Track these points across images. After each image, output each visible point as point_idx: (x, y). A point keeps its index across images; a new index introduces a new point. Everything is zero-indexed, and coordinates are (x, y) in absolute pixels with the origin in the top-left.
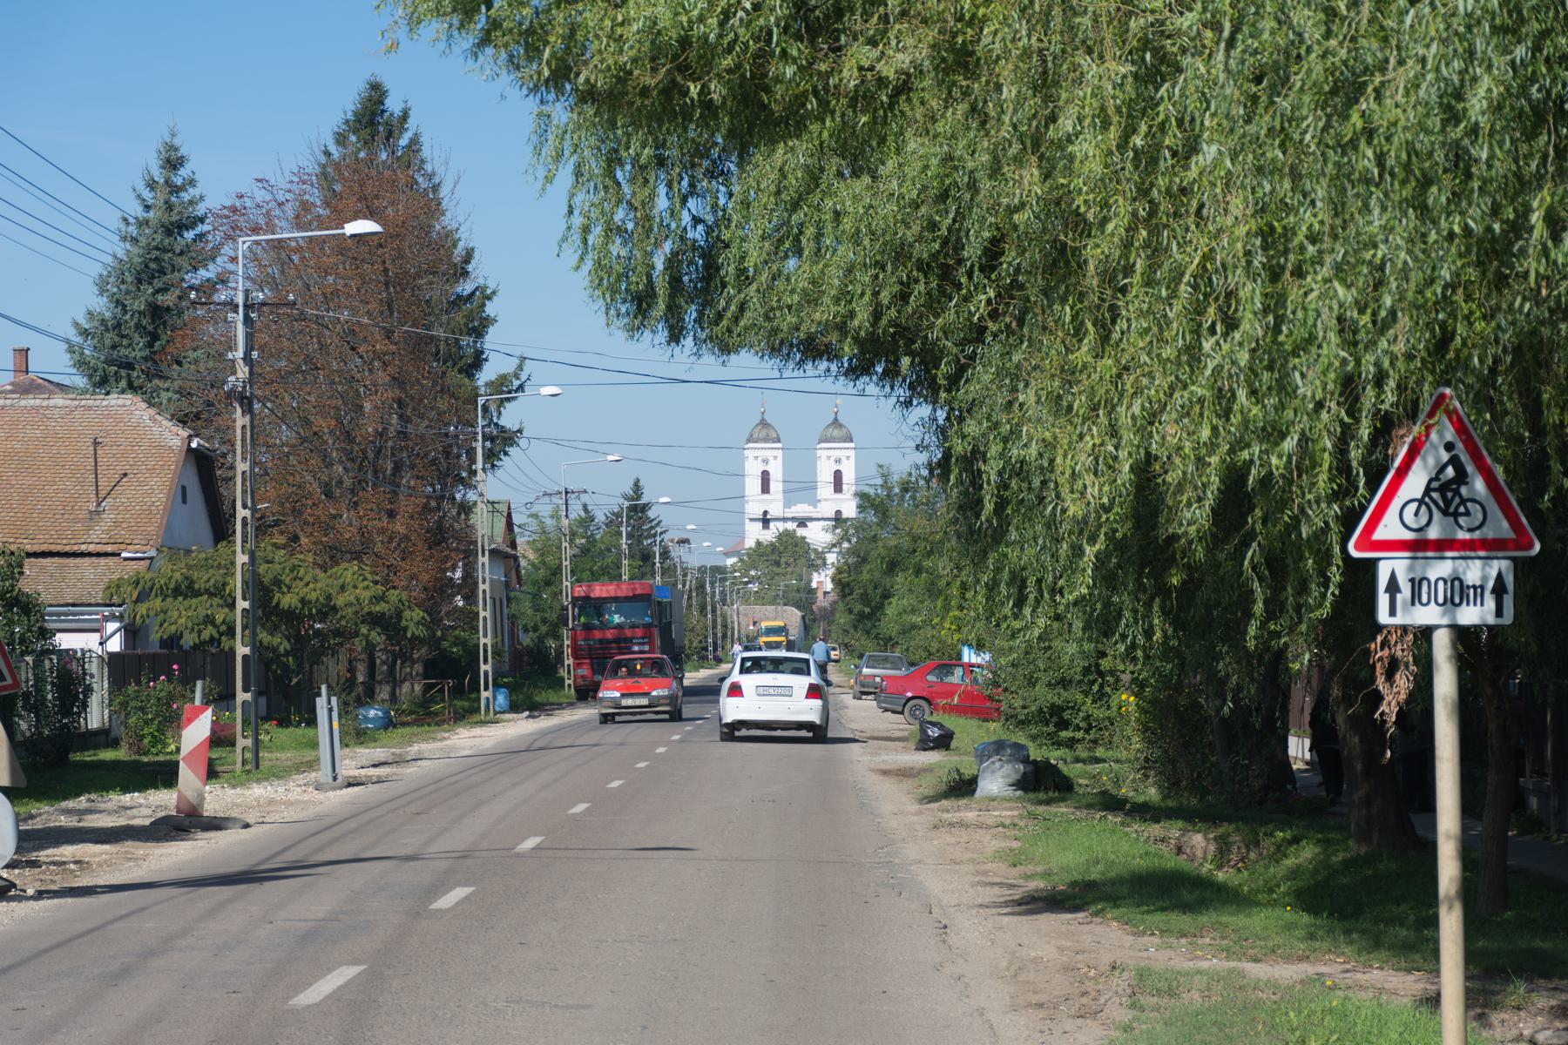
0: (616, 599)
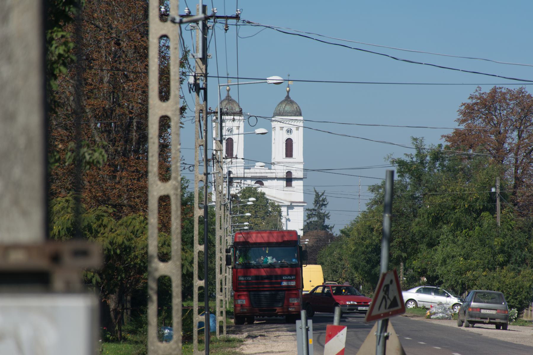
0: (269, 244)
